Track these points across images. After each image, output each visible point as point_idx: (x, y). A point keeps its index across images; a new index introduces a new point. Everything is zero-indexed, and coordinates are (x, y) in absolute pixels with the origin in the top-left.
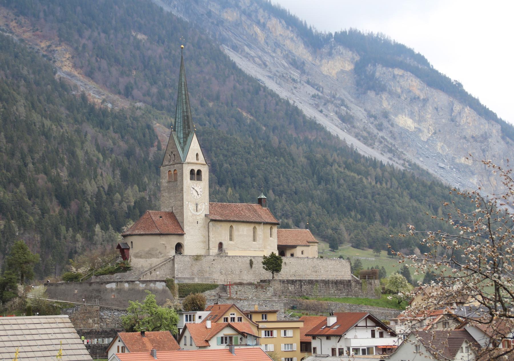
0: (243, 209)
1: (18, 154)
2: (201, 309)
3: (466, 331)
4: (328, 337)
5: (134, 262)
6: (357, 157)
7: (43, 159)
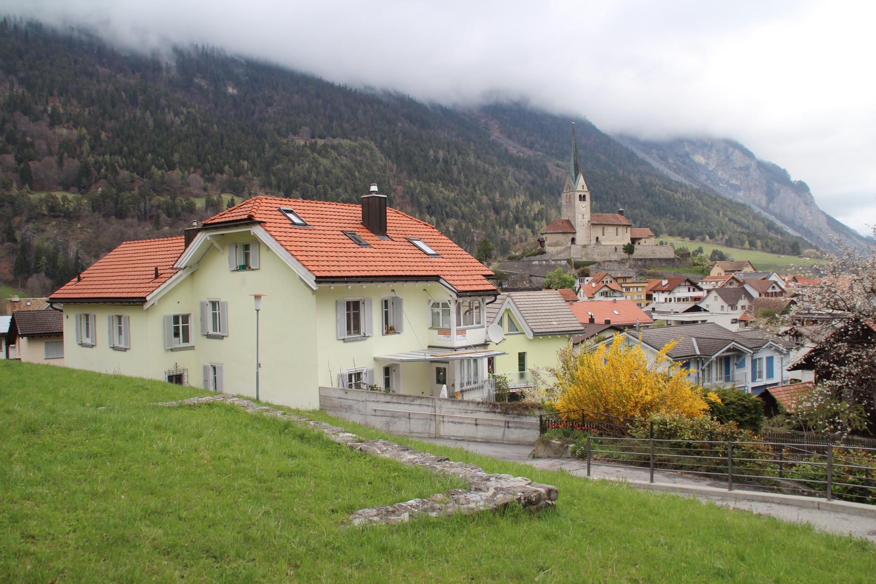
0: (610, 217)
1: (471, 185)
2: (588, 276)
3: (744, 288)
4: (663, 292)
5: (547, 249)
6: (670, 181)
7: (485, 188)
